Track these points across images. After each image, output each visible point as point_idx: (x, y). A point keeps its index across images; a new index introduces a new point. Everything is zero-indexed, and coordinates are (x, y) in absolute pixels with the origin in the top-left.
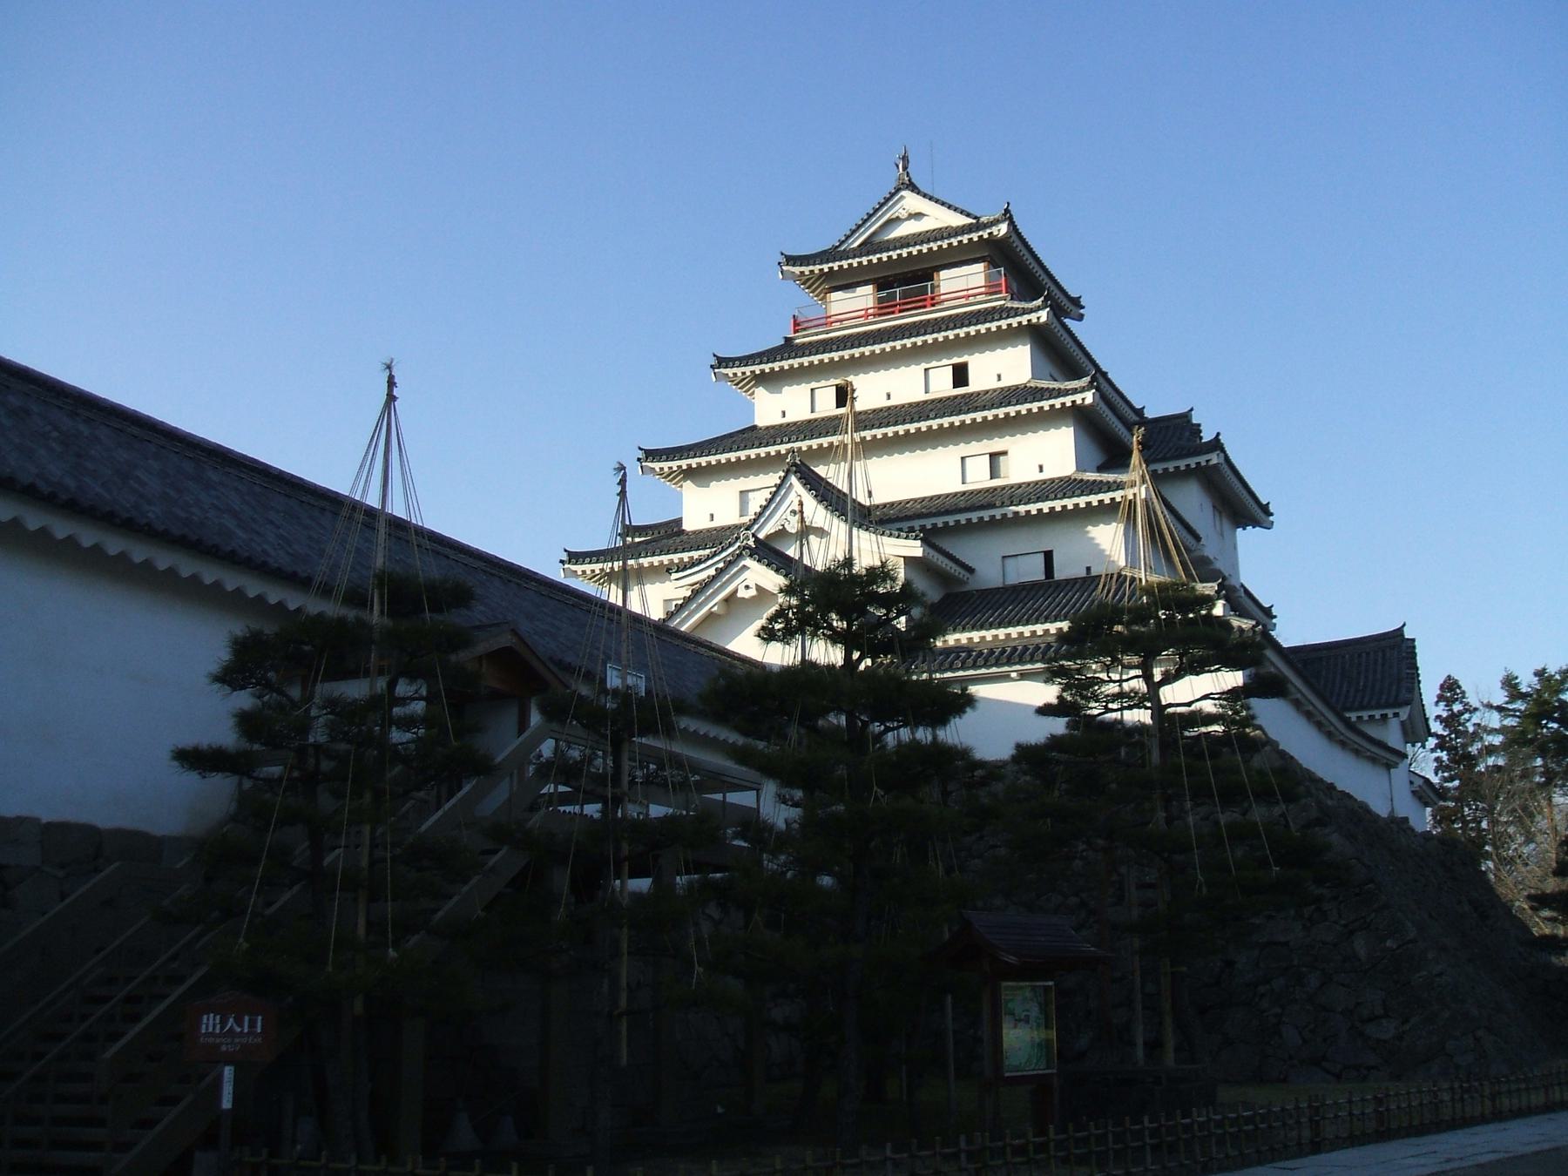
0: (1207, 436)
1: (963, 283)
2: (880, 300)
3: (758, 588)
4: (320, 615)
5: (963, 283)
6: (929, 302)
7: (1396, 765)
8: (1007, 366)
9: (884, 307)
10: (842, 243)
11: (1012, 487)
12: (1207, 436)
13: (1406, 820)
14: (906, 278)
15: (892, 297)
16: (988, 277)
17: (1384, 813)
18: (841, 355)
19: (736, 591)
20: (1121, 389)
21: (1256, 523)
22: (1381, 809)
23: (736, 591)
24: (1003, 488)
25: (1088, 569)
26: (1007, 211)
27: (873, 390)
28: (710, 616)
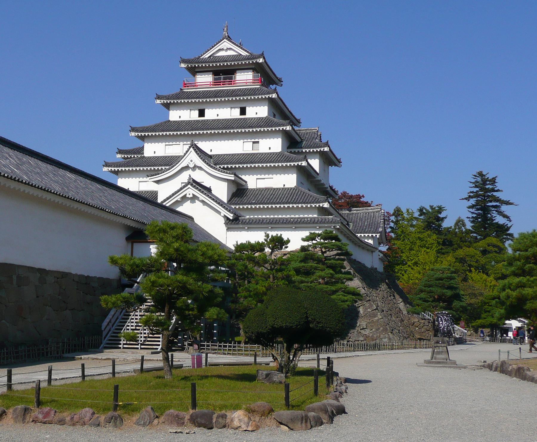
0: (324, 140)
1: (245, 78)
2: (215, 79)
3: (193, 194)
4: (240, 248)
5: (245, 78)
6: (233, 83)
7: (375, 252)
8: (259, 111)
9: (216, 82)
10: (202, 56)
11: (260, 154)
12: (324, 140)
13: (376, 269)
14: (224, 71)
15: (220, 79)
16: (254, 77)
17: (369, 267)
18: (201, 100)
19: (186, 194)
20: (294, 115)
21: (336, 165)
22: (369, 265)
23: (186, 194)
24: (257, 154)
25: (284, 185)
26: (263, 54)
27: (211, 114)
28: (177, 201)
